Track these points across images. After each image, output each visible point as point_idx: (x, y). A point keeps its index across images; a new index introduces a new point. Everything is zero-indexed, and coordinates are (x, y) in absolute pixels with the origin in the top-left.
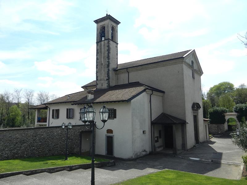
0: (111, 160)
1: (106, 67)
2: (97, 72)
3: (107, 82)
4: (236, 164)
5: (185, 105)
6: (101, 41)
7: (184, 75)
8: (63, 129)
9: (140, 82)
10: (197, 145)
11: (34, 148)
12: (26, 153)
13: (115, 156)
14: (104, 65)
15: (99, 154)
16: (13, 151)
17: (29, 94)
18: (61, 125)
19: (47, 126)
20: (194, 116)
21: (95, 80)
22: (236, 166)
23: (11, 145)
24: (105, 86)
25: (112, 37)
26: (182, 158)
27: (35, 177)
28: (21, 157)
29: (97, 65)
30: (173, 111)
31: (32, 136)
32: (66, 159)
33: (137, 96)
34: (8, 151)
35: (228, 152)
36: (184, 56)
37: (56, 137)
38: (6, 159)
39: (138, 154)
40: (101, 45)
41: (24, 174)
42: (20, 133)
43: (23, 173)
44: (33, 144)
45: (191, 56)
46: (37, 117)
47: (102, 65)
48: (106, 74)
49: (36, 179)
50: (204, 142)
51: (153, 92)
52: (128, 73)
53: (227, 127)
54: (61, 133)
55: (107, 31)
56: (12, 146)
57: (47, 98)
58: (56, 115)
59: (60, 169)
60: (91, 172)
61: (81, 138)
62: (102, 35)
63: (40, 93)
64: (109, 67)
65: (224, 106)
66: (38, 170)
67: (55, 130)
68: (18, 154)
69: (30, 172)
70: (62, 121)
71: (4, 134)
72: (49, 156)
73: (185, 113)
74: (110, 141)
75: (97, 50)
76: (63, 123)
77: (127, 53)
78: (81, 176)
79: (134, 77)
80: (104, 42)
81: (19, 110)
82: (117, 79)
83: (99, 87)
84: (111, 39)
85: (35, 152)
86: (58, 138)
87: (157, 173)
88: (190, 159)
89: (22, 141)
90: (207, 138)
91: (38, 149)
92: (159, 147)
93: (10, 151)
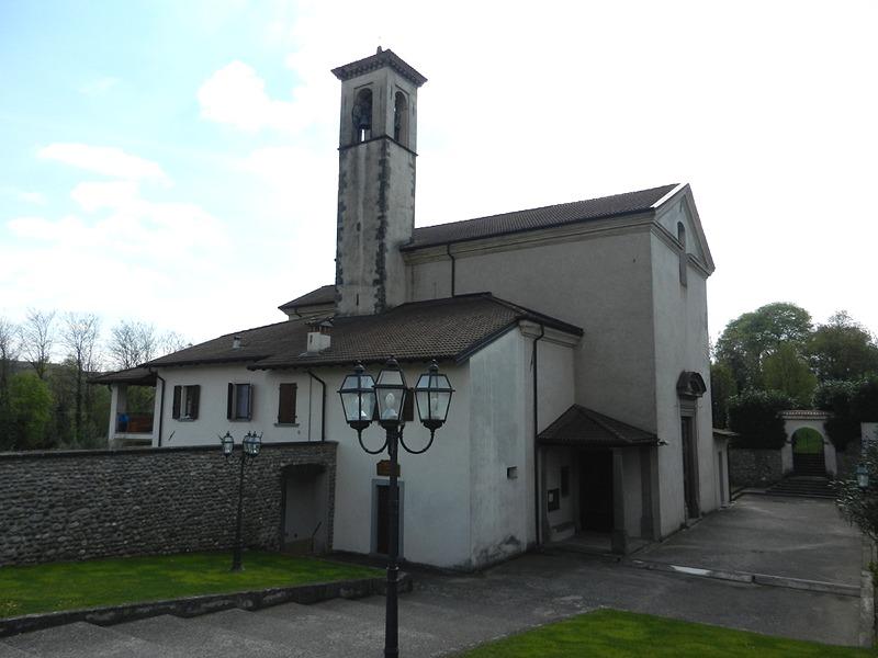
0: (388, 574)
1: (373, 239)
2: (339, 254)
3: (375, 290)
4: (838, 591)
5: (655, 378)
6: (356, 142)
7: (654, 271)
8: (227, 455)
9: (495, 294)
10: (692, 521)
11: (114, 524)
12: (84, 543)
13: (408, 559)
14: (366, 232)
15: (348, 550)
16: (38, 537)
17: (83, 333)
18: (219, 443)
19: (155, 445)
20: (683, 418)
21: (332, 281)
22: (840, 599)
23: (31, 513)
24: (368, 305)
25: (397, 129)
26: (647, 568)
27: (10, 644)
28: (68, 558)
29: (340, 230)
30: (612, 403)
31: (109, 480)
32: (236, 566)
33: (562, 323)
34: (19, 535)
35: (804, 547)
36: (655, 205)
37: (197, 484)
38: (14, 563)
39: (491, 551)
40: (356, 157)
41: (92, 621)
42: (65, 467)
43: (88, 617)
44: (111, 510)
45: (677, 207)
46: (118, 413)
47: (358, 229)
48: (374, 262)
49: (140, 641)
50: (714, 513)
51: (545, 328)
52: (453, 259)
53: (791, 461)
54: (211, 473)
55: (377, 105)
56: (34, 517)
57: (147, 347)
58: (189, 405)
59: (220, 603)
60: (383, 610)
61: (284, 492)
62: (359, 120)
63: (121, 327)
64: (383, 237)
65: (779, 387)
66: (140, 606)
67: (190, 460)
68: (57, 548)
69: (111, 614)
70: (211, 427)
71: (7, 471)
72: (167, 555)
73: (655, 408)
74: (388, 501)
75: (342, 176)
76: (228, 435)
77: (449, 187)
78: (302, 628)
79: (475, 274)
80: (368, 148)
81: (44, 387)
82: (413, 282)
83: (344, 307)
84: (392, 136)
85: (121, 538)
86: (202, 488)
87: (574, 619)
88: (675, 572)
89: (74, 501)
90: (722, 500)
91: (128, 531)
92: (561, 528)
93: (26, 535)
